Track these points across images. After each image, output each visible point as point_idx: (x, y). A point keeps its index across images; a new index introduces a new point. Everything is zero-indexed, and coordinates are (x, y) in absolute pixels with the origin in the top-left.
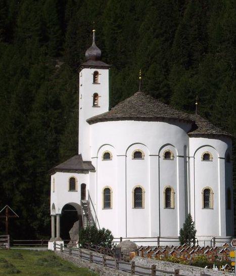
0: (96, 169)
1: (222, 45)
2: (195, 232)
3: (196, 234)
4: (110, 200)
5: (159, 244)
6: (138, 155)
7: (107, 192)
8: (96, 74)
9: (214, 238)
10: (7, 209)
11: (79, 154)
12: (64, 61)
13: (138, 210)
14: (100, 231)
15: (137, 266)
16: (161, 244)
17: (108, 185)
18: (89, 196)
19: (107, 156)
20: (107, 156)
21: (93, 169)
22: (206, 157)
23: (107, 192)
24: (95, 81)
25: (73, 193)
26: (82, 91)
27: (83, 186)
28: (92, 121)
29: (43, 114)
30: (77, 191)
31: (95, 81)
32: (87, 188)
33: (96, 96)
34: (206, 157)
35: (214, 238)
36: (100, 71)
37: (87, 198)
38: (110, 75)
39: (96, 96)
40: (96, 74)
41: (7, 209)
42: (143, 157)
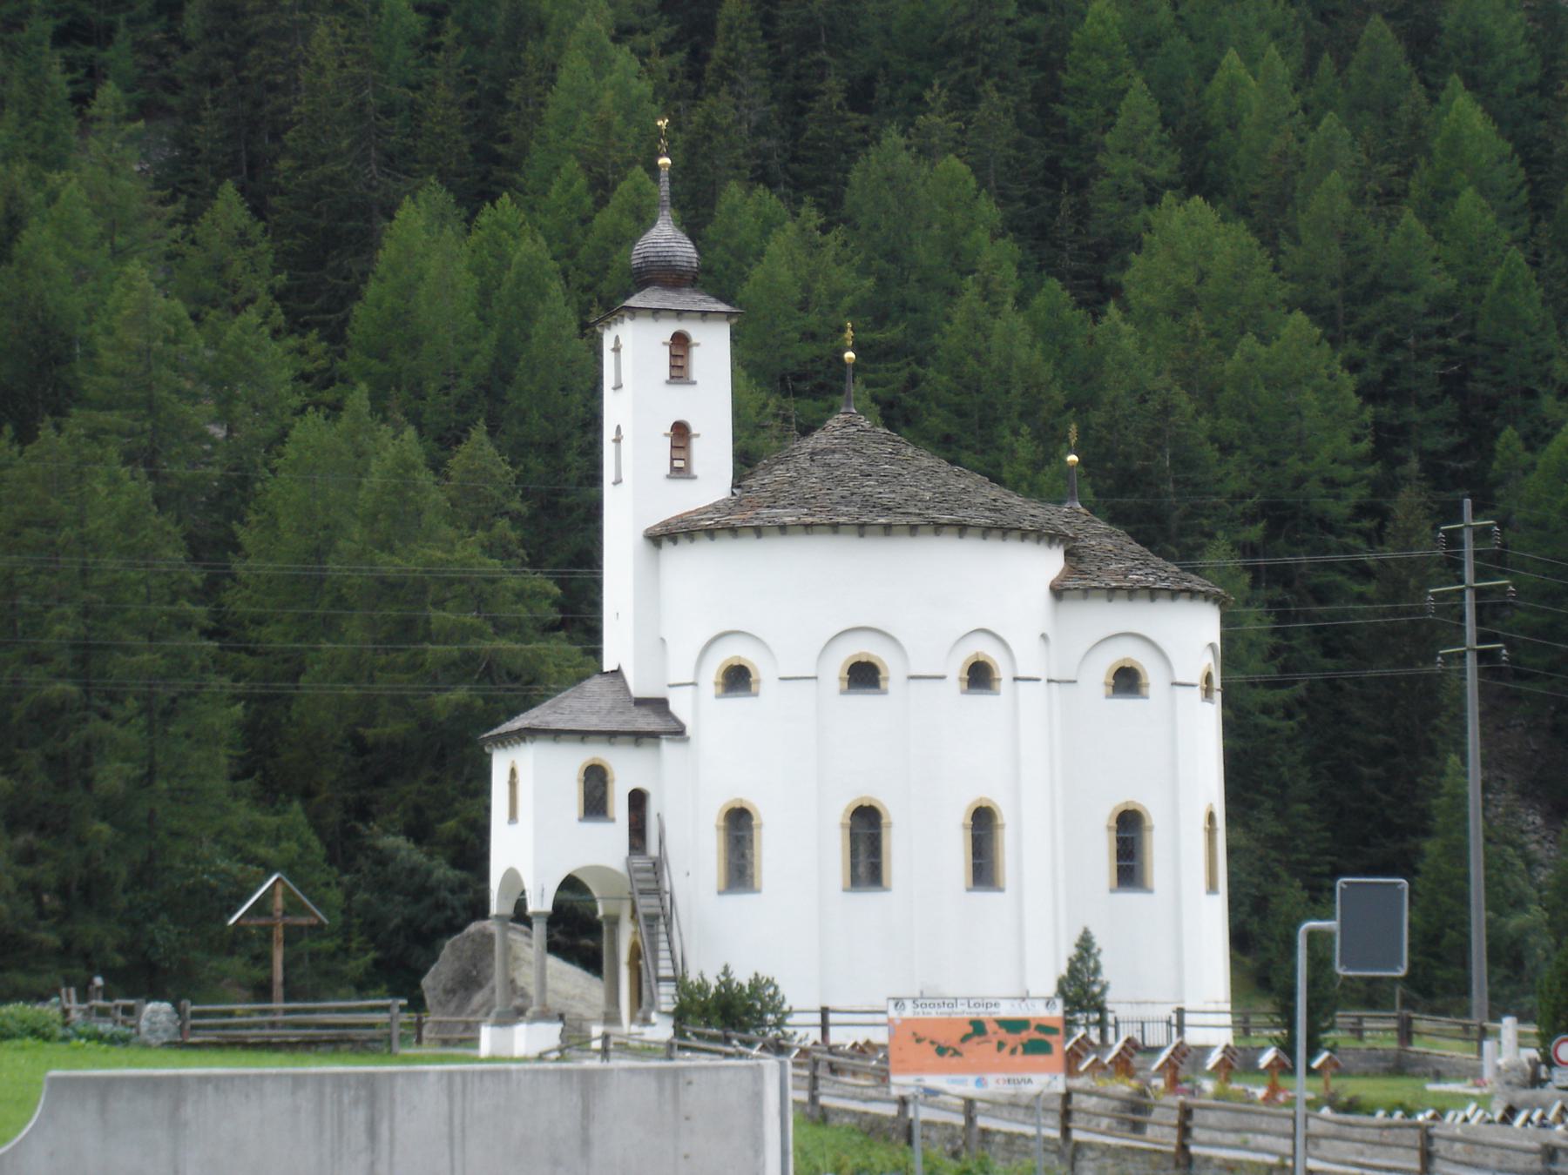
0: (689, 732)
1: (1260, 248)
4: (974, 865)
5: (825, 1032)
7: (739, 822)
8: (680, 343)
9: (825, 1012)
10: (279, 889)
11: (608, 665)
15: (1412, 1148)
16: (837, 1036)
17: (988, 796)
19: (737, 679)
20: (737, 679)
21: (678, 732)
23: (739, 822)
24: (679, 371)
25: (596, 828)
26: (615, 410)
27: (638, 800)
28: (662, 536)
29: (55, 502)
30: (613, 820)
31: (679, 371)
32: (653, 808)
33: (681, 433)
35: (825, 1012)
36: (696, 331)
37: (653, 848)
39: (681, 433)
40: (680, 343)
41: (279, 889)
42: (882, 684)
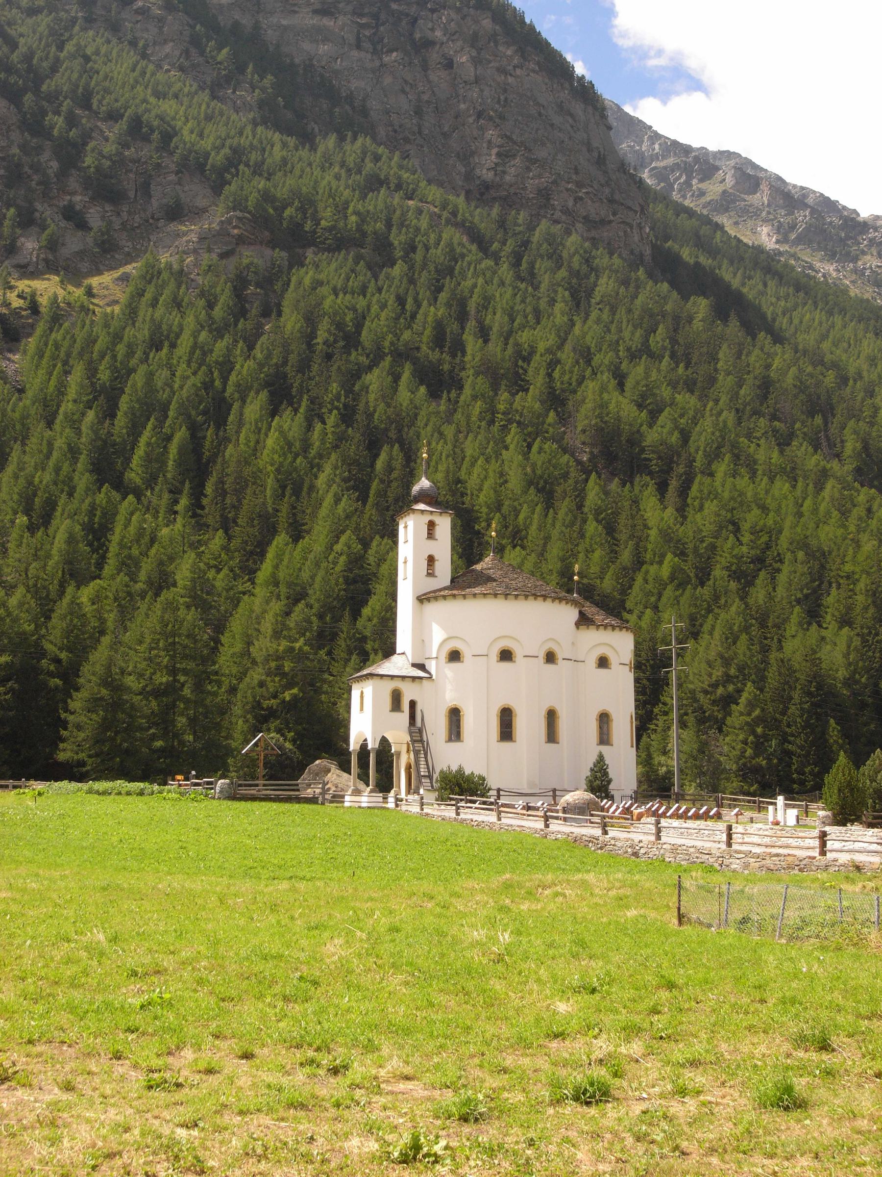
2: (460, 771)
3: (611, 787)
6: (506, 655)
7: (455, 715)
12: (615, 475)
13: (507, 745)
14: (774, 796)
18: (423, 720)
19: (455, 656)
20: (455, 656)
22: (603, 662)
23: (455, 715)
25: (396, 715)
27: (413, 704)
31: (431, 535)
32: (419, 708)
34: (603, 662)
36: (437, 519)
38: (453, 527)
39: (431, 560)
